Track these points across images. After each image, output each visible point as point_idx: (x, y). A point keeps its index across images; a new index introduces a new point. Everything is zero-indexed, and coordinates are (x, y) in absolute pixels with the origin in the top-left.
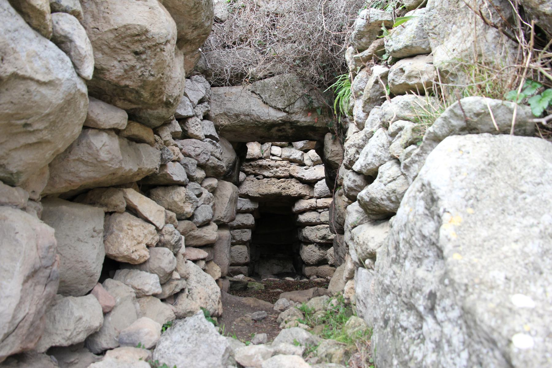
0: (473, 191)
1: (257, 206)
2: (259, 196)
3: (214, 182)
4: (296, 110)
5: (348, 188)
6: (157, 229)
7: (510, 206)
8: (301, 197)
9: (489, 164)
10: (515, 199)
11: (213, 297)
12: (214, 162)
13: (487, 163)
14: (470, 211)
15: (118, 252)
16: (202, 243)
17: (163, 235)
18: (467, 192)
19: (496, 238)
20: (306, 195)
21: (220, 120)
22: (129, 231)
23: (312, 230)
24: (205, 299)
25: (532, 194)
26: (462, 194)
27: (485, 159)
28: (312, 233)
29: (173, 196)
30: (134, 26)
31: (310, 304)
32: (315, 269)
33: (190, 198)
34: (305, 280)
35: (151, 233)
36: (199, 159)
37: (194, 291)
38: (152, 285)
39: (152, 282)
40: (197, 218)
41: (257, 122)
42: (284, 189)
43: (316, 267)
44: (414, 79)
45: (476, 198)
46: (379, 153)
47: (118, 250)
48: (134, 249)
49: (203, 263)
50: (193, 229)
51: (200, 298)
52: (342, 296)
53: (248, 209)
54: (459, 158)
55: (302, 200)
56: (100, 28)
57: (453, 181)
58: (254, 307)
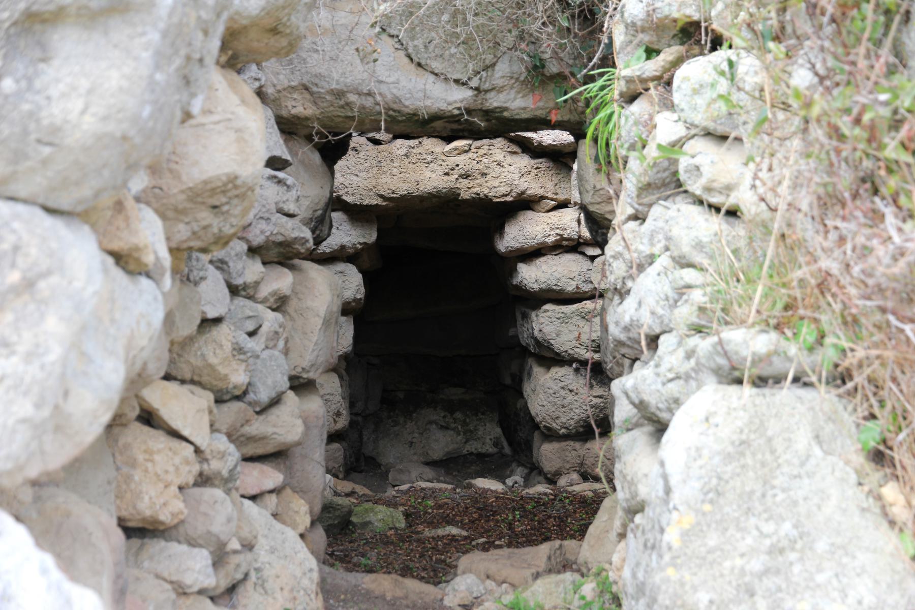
0: (714, 481)
1: (370, 236)
2: (380, 202)
3: (281, 281)
4: (500, 82)
5: (615, 340)
6: (198, 451)
7: (757, 504)
8: (525, 204)
9: (740, 444)
10: (764, 496)
11: (306, 582)
12: (282, 231)
13: (737, 443)
14: (707, 507)
15: (134, 512)
16: (270, 449)
17: (207, 460)
18: (706, 483)
19: (722, 550)
20: (543, 198)
21: (290, 104)
22: (149, 465)
23: (566, 317)
24: (292, 590)
25: (784, 490)
26: (697, 485)
27: (735, 437)
28: (564, 329)
29: (204, 349)
30: (218, 178)
31: (533, 594)
32: (574, 451)
33: (241, 349)
34: (541, 488)
35: (187, 462)
36: (250, 236)
37: (268, 573)
38: (199, 572)
39: (198, 567)
40: (255, 393)
41: (394, 111)
42: (466, 176)
43: (577, 445)
44: (717, 194)
45: (717, 491)
46: (660, 311)
47: (134, 507)
48: (162, 501)
49: (272, 500)
50: (247, 421)
51: (282, 589)
52: (607, 577)
53: (343, 247)
54: (702, 434)
55: (530, 214)
56: (165, 188)
57: (689, 468)
58: (395, 599)
